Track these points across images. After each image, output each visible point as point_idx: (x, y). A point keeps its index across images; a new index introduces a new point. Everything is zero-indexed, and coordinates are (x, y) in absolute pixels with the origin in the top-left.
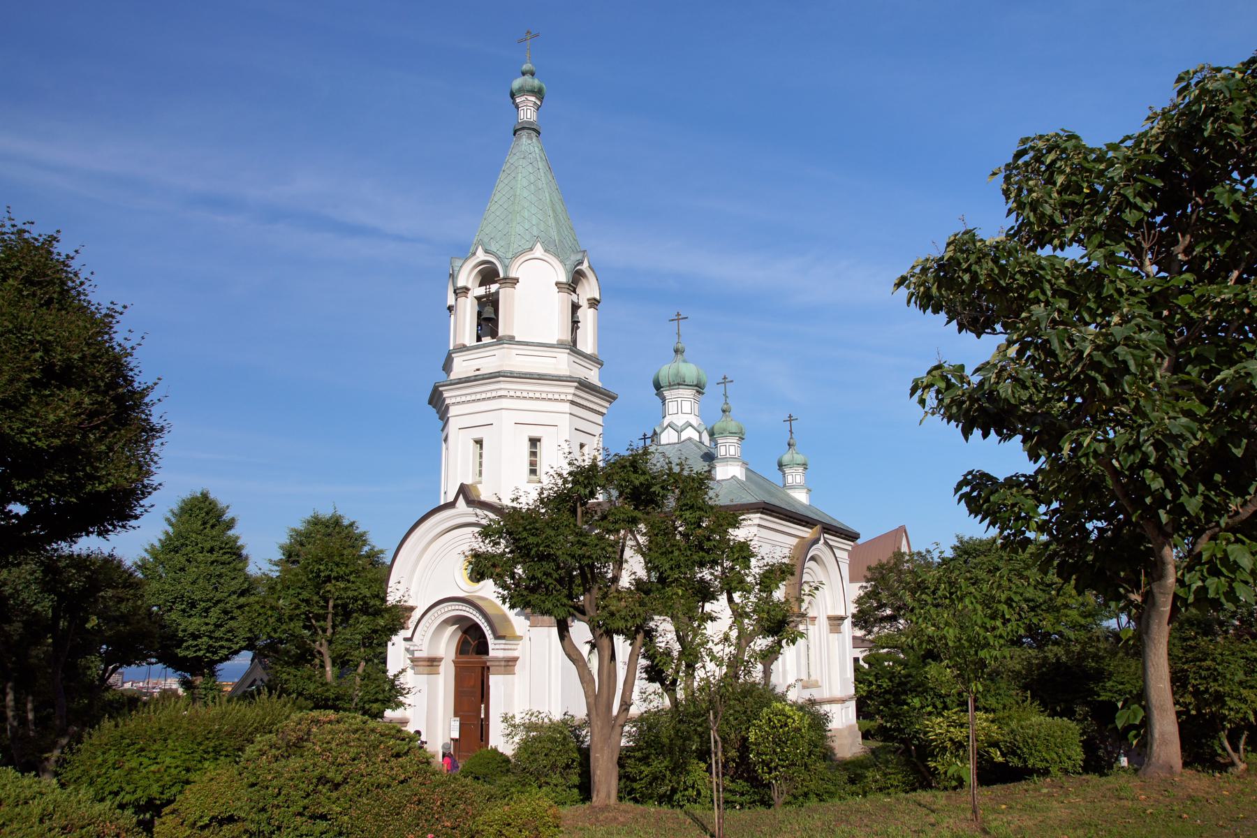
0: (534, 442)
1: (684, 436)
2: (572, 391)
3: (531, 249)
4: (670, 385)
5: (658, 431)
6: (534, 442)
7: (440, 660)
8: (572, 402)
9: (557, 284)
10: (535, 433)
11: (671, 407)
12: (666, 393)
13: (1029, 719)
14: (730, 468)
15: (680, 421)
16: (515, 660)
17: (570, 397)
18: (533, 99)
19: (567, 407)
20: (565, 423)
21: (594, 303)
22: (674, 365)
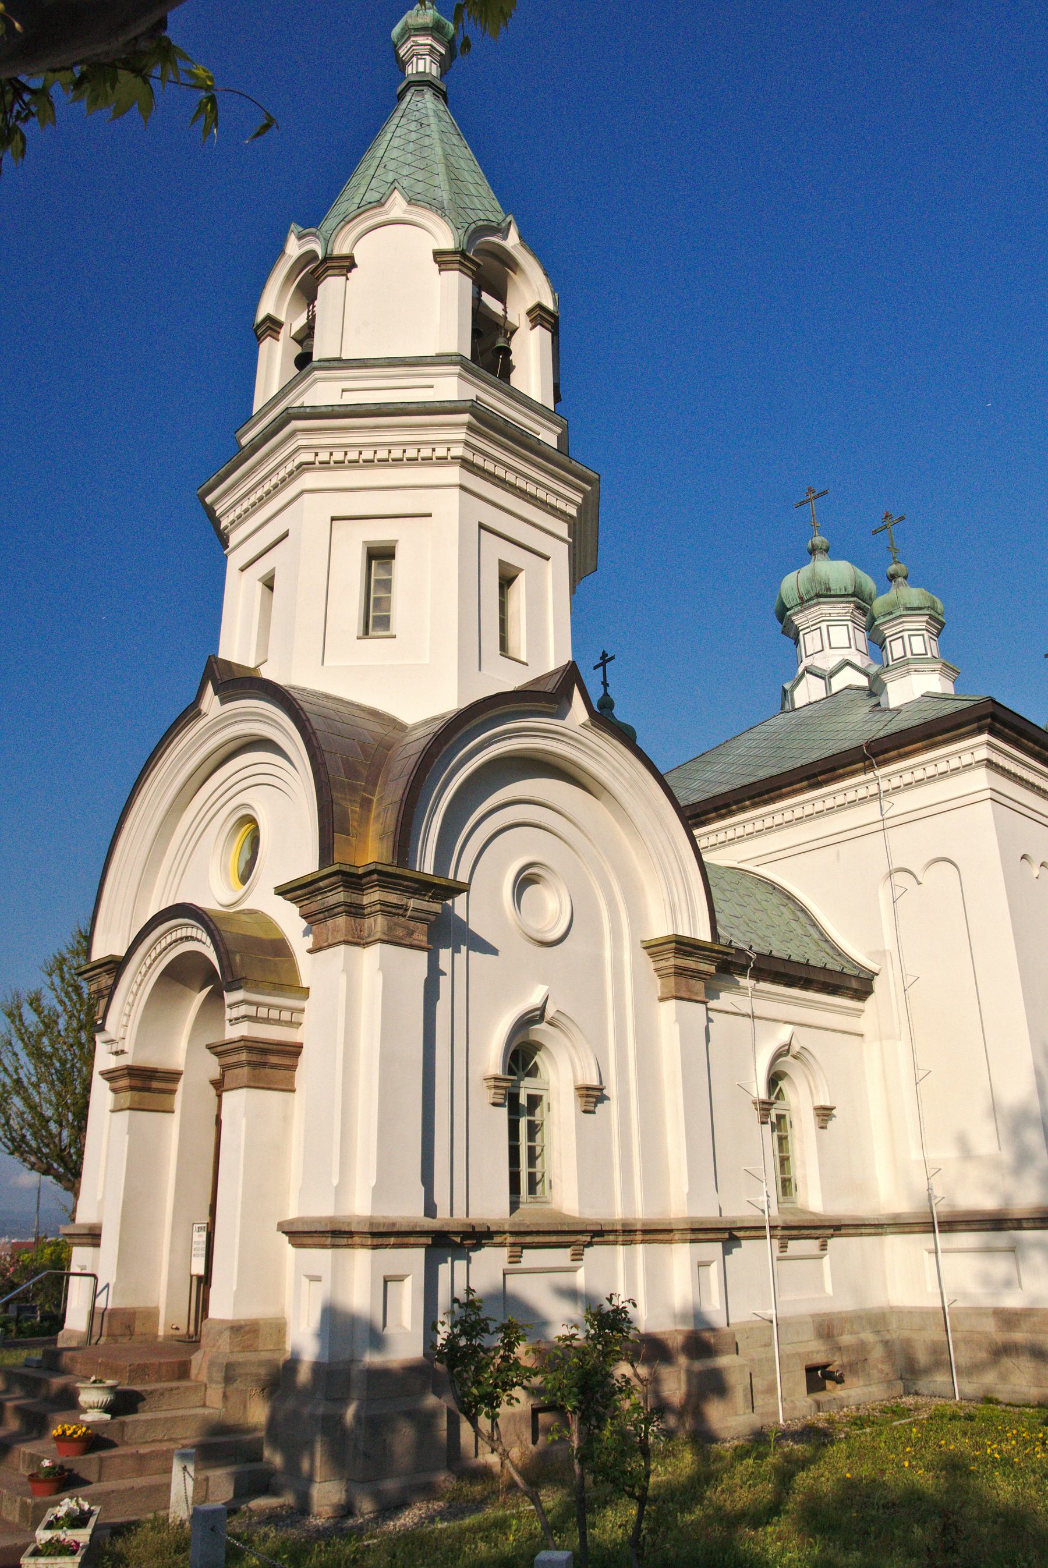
0: (380, 555)
1: (838, 683)
2: (461, 434)
3: (380, 203)
4: (803, 601)
5: (787, 686)
6: (380, 555)
7: (174, 1076)
8: (466, 464)
9: (437, 254)
10: (380, 533)
11: (810, 642)
12: (798, 620)
13: (517, 1506)
14: (915, 678)
15: (827, 661)
16: (294, 1051)
17: (458, 451)
18: (429, 41)
19: (453, 474)
20: (448, 505)
21: (539, 315)
22: (805, 571)
